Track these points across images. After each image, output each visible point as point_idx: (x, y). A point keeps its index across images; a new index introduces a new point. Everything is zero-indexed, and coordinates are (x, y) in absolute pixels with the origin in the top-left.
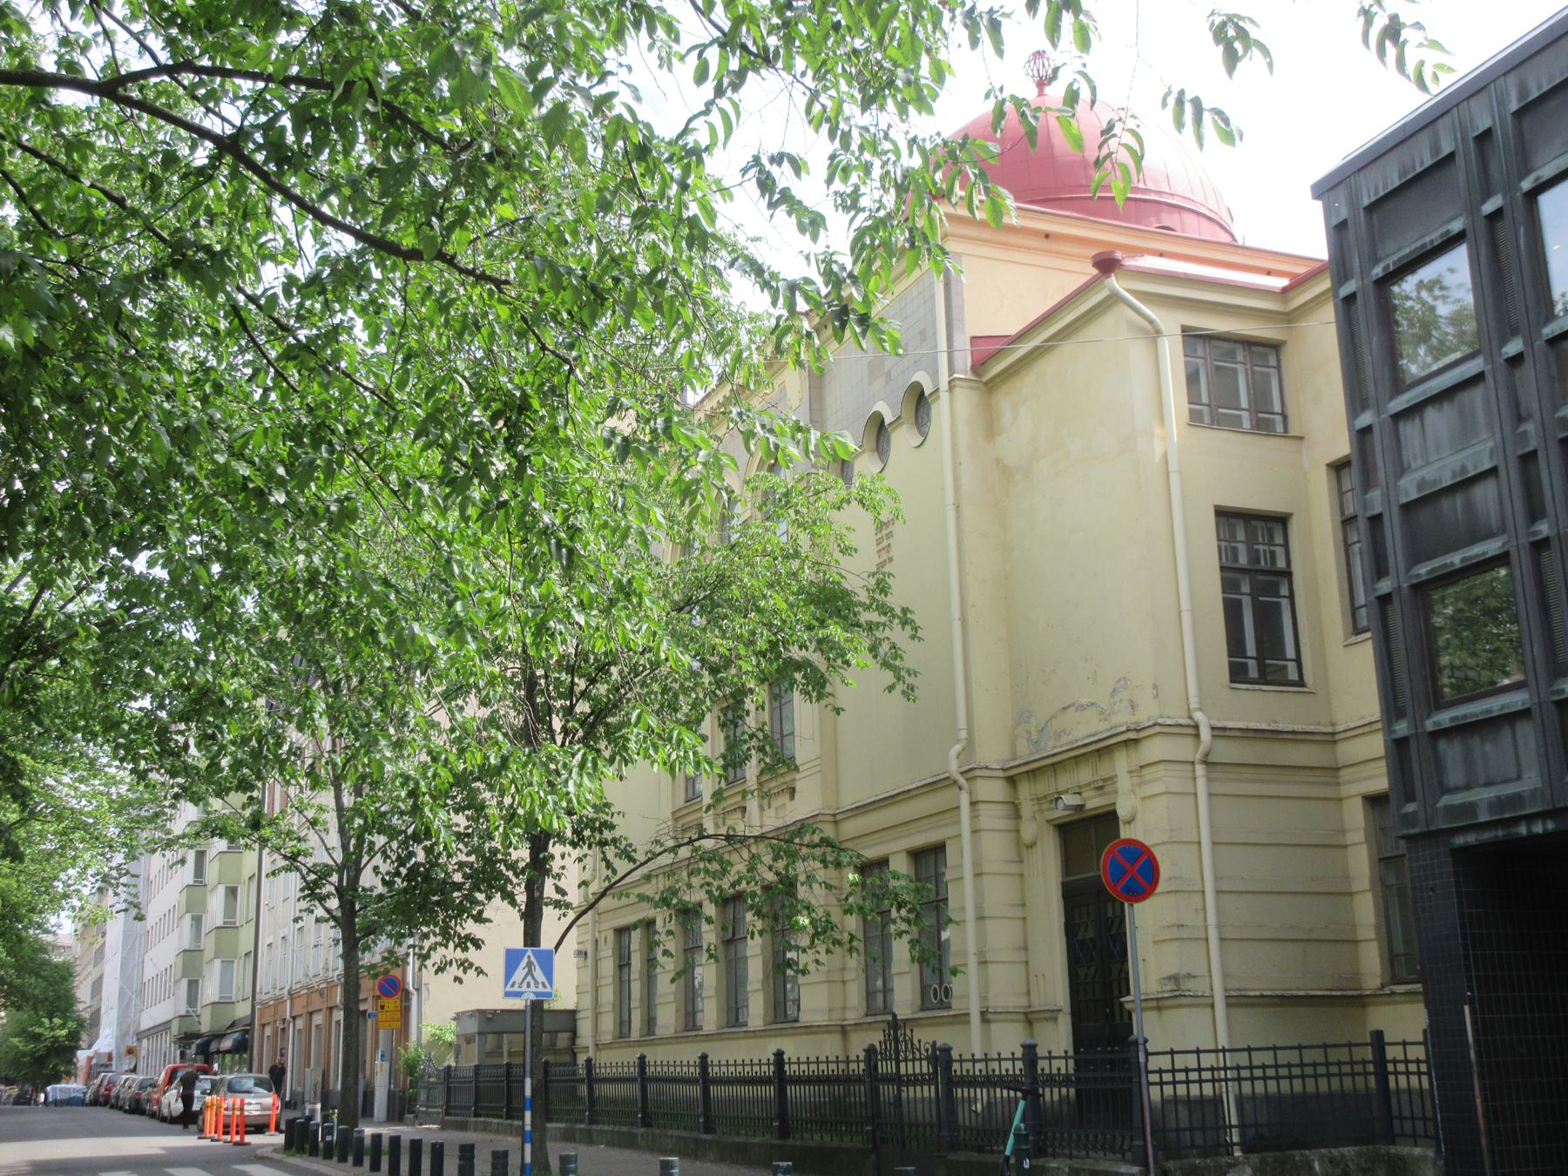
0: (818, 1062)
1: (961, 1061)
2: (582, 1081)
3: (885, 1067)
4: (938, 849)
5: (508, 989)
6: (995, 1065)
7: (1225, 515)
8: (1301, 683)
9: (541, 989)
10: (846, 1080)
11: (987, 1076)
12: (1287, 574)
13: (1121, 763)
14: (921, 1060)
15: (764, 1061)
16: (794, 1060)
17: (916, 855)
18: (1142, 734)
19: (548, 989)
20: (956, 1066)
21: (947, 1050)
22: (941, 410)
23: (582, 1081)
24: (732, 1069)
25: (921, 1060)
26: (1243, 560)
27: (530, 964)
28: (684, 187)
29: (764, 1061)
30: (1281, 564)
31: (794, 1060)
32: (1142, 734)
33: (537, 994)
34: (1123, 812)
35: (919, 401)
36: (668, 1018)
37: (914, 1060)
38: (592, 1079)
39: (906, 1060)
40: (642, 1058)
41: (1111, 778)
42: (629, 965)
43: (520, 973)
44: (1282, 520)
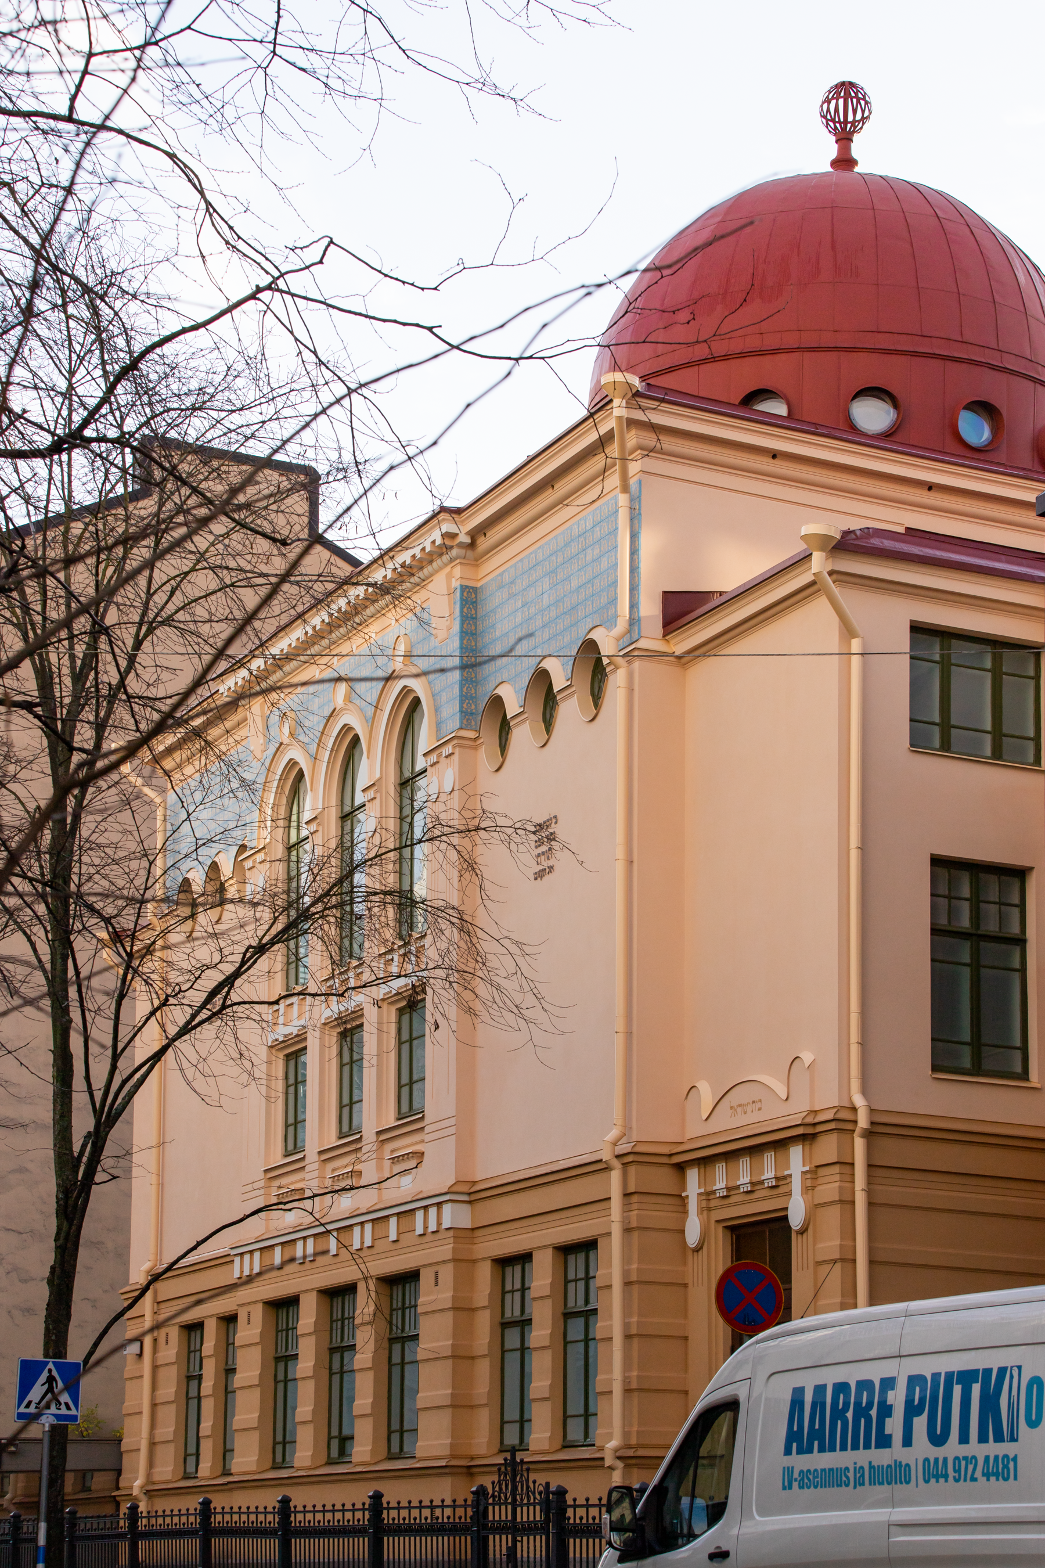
0: (421, 1507)
1: (575, 1507)
2: (122, 1536)
3: (497, 1514)
4: (589, 1246)
5: (22, 1410)
6: (153, 1521)
7: (937, 862)
8: (1025, 1075)
9: (64, 1411)
10: (452, 1529)
11: (432, 1525)
12: (1021, 941)
13: (797, 1160)
14: (534, 1505)
15: (594, 1501)
16: (581, 1501)
17: (565, 1250)
18: (819, 1128)
19: (73, 1412)
20: (570, 1512)
21: (562, 1492)
22: (617, 682)
23: (122, 1536)
24: (415, 1513)
25: (534, 1505)
26: (965, 922)
27: (51, 1379)
28: (59, 411)
29: (594, 1501)
30: (1016, 929)
31: (581, 1501)
32: (819, 1128)
33: (58, 1417)
34: (796, 1218)
35: (593, 666)
36: (247, 1458)
37: (528, 1505)
38: (135, 1535)
39: (522, 1506)
40: (377, 1497)
41: (785, 1178)
42: (200, 1377)
43: (37, 1392)
44: (1020, 874)
